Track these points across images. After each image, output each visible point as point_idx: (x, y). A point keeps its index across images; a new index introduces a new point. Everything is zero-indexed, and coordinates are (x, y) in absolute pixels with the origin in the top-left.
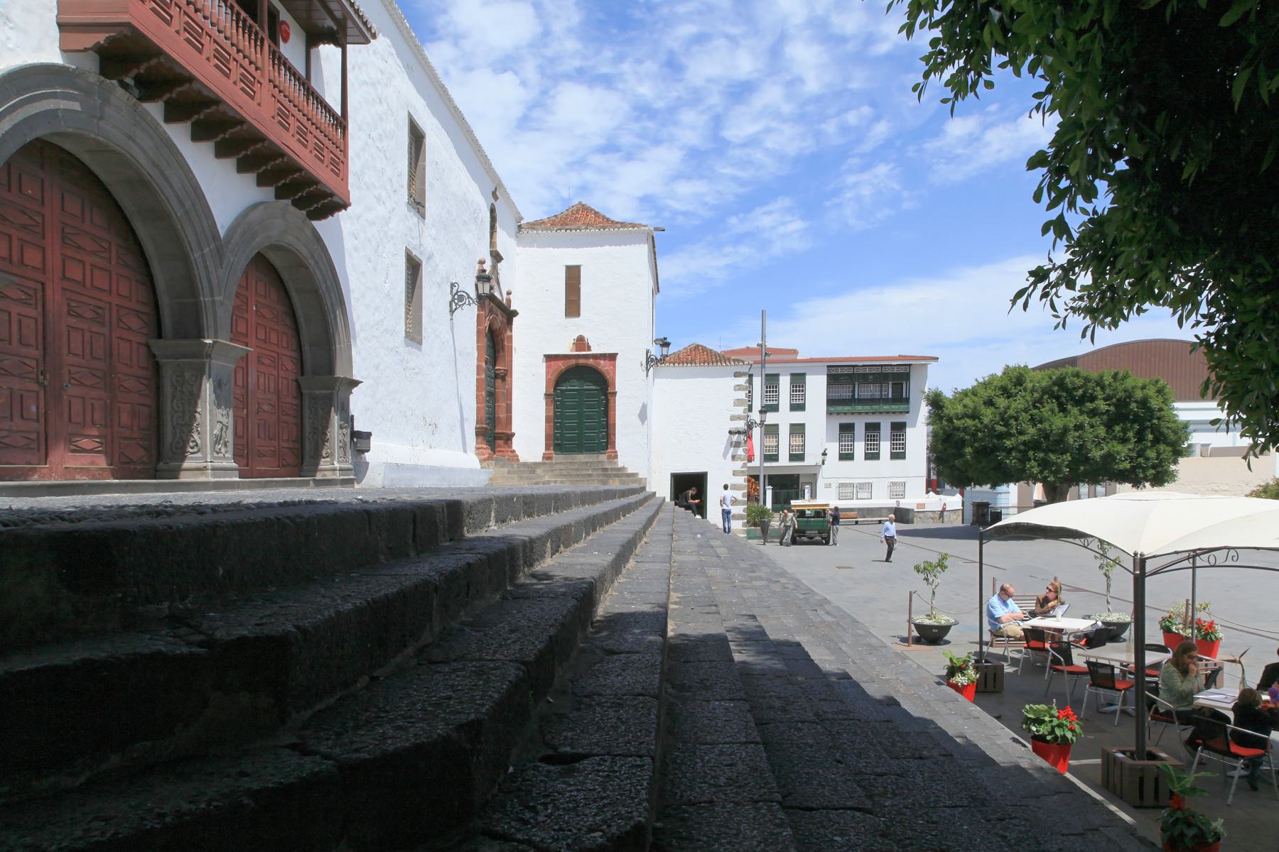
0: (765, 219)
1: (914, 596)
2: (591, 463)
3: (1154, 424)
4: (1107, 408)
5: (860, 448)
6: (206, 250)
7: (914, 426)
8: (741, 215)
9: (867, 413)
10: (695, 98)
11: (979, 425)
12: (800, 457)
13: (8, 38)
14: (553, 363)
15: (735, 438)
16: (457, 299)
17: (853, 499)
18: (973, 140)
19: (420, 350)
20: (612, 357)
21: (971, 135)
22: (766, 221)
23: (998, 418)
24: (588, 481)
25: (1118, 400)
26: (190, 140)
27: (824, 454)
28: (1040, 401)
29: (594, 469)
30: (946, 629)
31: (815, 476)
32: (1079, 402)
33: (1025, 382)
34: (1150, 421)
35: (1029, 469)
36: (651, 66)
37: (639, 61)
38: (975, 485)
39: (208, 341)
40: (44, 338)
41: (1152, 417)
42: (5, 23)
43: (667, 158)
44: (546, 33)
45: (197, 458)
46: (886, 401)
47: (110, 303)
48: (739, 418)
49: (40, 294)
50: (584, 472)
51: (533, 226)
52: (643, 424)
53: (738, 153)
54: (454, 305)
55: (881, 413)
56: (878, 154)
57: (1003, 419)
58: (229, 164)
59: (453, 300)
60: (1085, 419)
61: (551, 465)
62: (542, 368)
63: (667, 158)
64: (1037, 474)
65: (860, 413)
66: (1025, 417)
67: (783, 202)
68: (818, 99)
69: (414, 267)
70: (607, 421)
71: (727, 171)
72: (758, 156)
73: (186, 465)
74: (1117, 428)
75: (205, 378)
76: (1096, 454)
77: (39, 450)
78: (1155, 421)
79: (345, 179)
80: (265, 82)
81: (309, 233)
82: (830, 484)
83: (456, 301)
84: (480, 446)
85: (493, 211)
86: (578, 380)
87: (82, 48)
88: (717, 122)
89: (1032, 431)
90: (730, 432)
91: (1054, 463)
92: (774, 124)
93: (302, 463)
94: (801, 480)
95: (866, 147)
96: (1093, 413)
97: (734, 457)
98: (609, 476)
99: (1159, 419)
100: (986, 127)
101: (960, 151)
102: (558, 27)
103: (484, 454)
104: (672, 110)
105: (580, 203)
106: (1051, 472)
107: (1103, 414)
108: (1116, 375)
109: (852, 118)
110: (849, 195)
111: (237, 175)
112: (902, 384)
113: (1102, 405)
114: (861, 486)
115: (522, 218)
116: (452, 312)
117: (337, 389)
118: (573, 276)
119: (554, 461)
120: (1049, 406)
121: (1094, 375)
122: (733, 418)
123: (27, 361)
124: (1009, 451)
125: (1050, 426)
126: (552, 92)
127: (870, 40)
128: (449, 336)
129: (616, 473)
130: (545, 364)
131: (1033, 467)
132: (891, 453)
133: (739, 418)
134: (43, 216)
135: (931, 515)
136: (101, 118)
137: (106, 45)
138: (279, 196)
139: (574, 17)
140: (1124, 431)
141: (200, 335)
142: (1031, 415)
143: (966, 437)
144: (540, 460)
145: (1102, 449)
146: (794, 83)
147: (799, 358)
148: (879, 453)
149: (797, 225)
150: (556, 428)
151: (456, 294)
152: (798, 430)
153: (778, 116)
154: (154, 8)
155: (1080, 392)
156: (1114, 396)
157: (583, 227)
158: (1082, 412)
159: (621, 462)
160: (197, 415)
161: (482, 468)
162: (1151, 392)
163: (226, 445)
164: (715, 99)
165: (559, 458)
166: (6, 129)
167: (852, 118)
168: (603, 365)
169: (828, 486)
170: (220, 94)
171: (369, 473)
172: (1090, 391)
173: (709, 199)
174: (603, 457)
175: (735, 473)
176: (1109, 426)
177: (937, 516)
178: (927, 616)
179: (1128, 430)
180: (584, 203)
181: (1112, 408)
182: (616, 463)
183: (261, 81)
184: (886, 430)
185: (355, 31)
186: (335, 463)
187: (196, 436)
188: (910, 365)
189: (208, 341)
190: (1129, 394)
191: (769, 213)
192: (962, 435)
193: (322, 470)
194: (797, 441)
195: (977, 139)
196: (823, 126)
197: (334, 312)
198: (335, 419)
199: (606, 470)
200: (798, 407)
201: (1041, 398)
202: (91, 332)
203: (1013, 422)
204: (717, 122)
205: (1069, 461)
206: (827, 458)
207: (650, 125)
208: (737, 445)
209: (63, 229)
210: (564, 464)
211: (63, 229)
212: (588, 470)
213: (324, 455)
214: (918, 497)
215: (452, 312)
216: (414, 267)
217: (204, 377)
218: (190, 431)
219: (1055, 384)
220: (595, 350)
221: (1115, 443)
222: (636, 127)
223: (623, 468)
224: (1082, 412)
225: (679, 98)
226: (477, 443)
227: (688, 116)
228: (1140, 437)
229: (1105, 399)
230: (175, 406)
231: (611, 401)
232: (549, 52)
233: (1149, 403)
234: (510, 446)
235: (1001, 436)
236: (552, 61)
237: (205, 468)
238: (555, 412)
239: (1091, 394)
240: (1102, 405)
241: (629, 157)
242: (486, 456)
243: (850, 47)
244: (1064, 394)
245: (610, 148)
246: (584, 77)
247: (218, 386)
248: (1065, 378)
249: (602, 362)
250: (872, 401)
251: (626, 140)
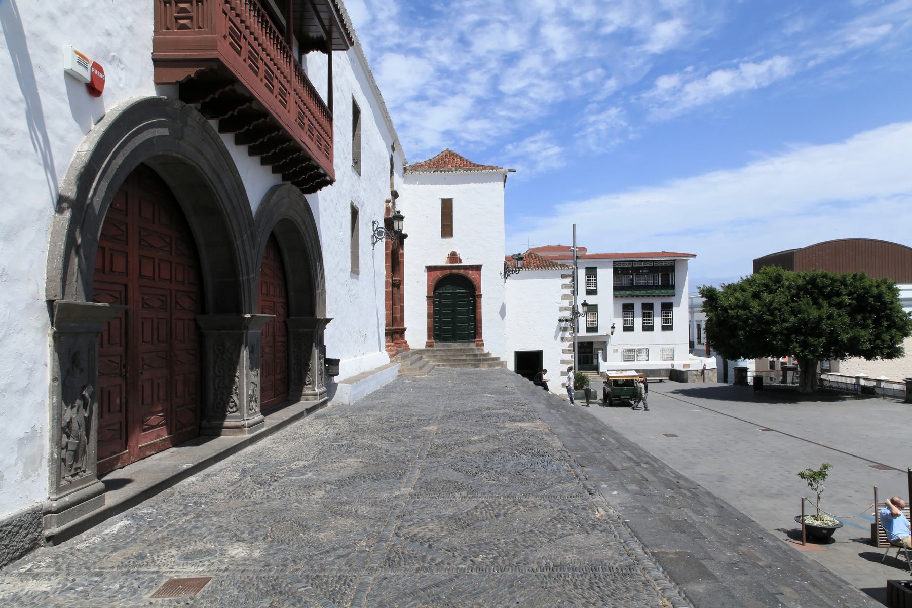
0: (532, 146)
1: (806, 502)
2: (465, 350)
3: (887, 313)
4: (850, 301)
5: (638, 322)
6: (245, 237)
7: (679, 305)
8: (515, 144)
9: (643, 296)
10: (479, 64)
11: (749, 314)
12: (595, 330)
13: (120, 79)
14: (432, 272)
15: (563, 324)
16: (377, 234)
17: (634, 361)
18: (676, 91)
19: (358, 279)
20: (478, 268)
21: (674, 87)
22: (533, 148)
23: (765, 309)
24: (464, 364)
25: (858, 295)
26: (234, 144)
27: (613, 327)
28: (797, 295)
29: (467, 355)
30: (832, 530)
31: (605, 343)
32: (828, 297)
33: (782, 280)
34: (884, 311)
35: (792, 349)
36: (448, 42)
37: (440, 39)
38: (745, 358)
39: (248, 316)
40: (126, 333)
41: (885, 309)
42: (118, 65)
43: (460, 104)
44: (374, 20)
45: (236, 417)
46: (657, 287)
47: (171, 290)
48: (566, 309)
49: (123, 294)
50: (459, 358)
51: (416, 167)
52: (503, 319)
53: (511, 101)
54: (375, 238)
55: (654, 296)
56: (611, 101)
57: (769, 310)
58: (257, 159)
59: (374, 234)
60: (835, 311)
61: (433, 351)
62: (424, 276)
63: (460, 104)
64: (799, 353)
65: (638, 296)
66: (786, 309)
67: (544, 135)
68: (565, 64)
69: (355, 213)
70: (475, 317)
71: (504, 113)
72: (525, 103)
73: (227, 423)
74: (859, 317)
75: (243, 346)
76: (844, 337)
77: (120, 439)
78: (888, 311)
79: (331, 161)
80: (292, 92)
81: (302, 204)
82: (617, 350)
83: (377, 235)
84: (389, 344)
85: (392, 160)
86: (452, 285)
87: (174, 81)
88: (496, 80)
89: (793, 319)
90: (560, 320)
91: (813, 345)
92: (535, 81)
93: (288, 390)
94: (595, 346)
95: (601, 97)
96: (840, 305)
97: (562, 339)
98: (480, 360)
99: (890, 309)
100: (685, 82)
101: (667, 99)
102: (382, 16)
103: (392, 351)
104: (464, 72)
105: (447, 150)
106: (810, 351)
107: (848, 306)
108: (855, 276)
109: (590, 76)
110: (591, 129)
111: (261, 166)
112: (669, 274)
113: (847, 300)
114: (641, 351)
115: (407, 163)
116: (374, 244)
117: (317, 327)
118: (447, 206)
119: (435, 348)
120: (805, 302)
121: (838, 276)
122: (561, 309)
123: (113, 359)
124: (775, 335)
125: (808, 316)
126: (379, 60)
127: (599, 24)
128: (371, 263)
129: (484, 358)
130: (426, 273)
131: (796, 348)
132: (662, 326)
133: (566, 309)
134: (127, 225)
135: (695, 373)
136: (181, 139)
137: (195, 78)
138: (284, 179)
139: (394, 9)
140: (864, 319)
141: (239, 311)
142: (791, 307)
143: (739, 323)
144: (423, 347)
145: (848, 333)
146: (548, 53)
147: (588, 254)
148: (653, 326)
149: (555, 150)
150: (435, 322)
151: (377, 229)
152: (592, 309)
153: (537, 75)
154: (231, 42)
155: (829, 289)
156: (855, 292)
157: (454, 169)
158: (830, 305)
159: (486, 349)
160: (236, 379)
161: (391, 362)
162: (883, 288)
163: (256, 401)
164: (493, 65)
165: (438, 346)
166: (120, 163)
167: (590, 76)
168: (471, 274)
169: (616, 351)
170: (269, 109)
171: (338, 393)
172: (836, 289)
173: (491, 133)
174: (472, 345)
175: (564, 351)
176: (851, 314)
177: (700, 374)
178: (813, 516)
179: (867, 318)
180: (450, 150)
181: (854, 302)
182: (482, 349)
183: (290, 92)
184: (657, 308)
185: (341, 41)
186: (316, 389)
187: (235, 398)
188: (674, 261)
189: (248, 316)
190: (867, 290)
191: (535, 142)
192: (736, 321)
193: (305, 395)
194: (592, 317)
195: (679, 90)
196: (570, 82)
197: (316, 265)
198: (316, 352)
199: (476, 355)
200: (592, 292)
201: (798, 294)
202: (157, 318)
203: (777, 312)
204: (496, 80)
205: (824, 343)
206: (615, 330)
207: (449, 82)
208: (565, 329)
209: (140, 232)
210: (443, 350)
211: (140, 232)
212: (462, 355)
213: (307, 382)
214: (685, 360)
215: (374, 244)
216: (355, 213)
217: (243, 346)
218: (230, 393)
219: (808, 283)
220: (465, 263)
221: (859, 329)
222: (439, 83)
223: (488, 354)
224: (830, 305)
225: (468, 64)
226: (386, 342)
227: (475, 76)
228: (877, 323)
229: (848, 295)
230: (217, 373)
231: (478, 301)
232: (376, 33)
233: (884, 297)
234: (403, 339)
235: (768, 323)
236: (378, 39)
237: (243, 426)
238: (434, 310)
239: (837, 291)
240: (847, 300)
241: (434, 104)
242: (394, 352)
243: (586, 29)
244: (816, 291)
245: (420, 97)
246: (399, 49)
247: (252, 352)
248: (816, 279)
249: (470, 272)
250: (646, 287)
251: (432, 92)
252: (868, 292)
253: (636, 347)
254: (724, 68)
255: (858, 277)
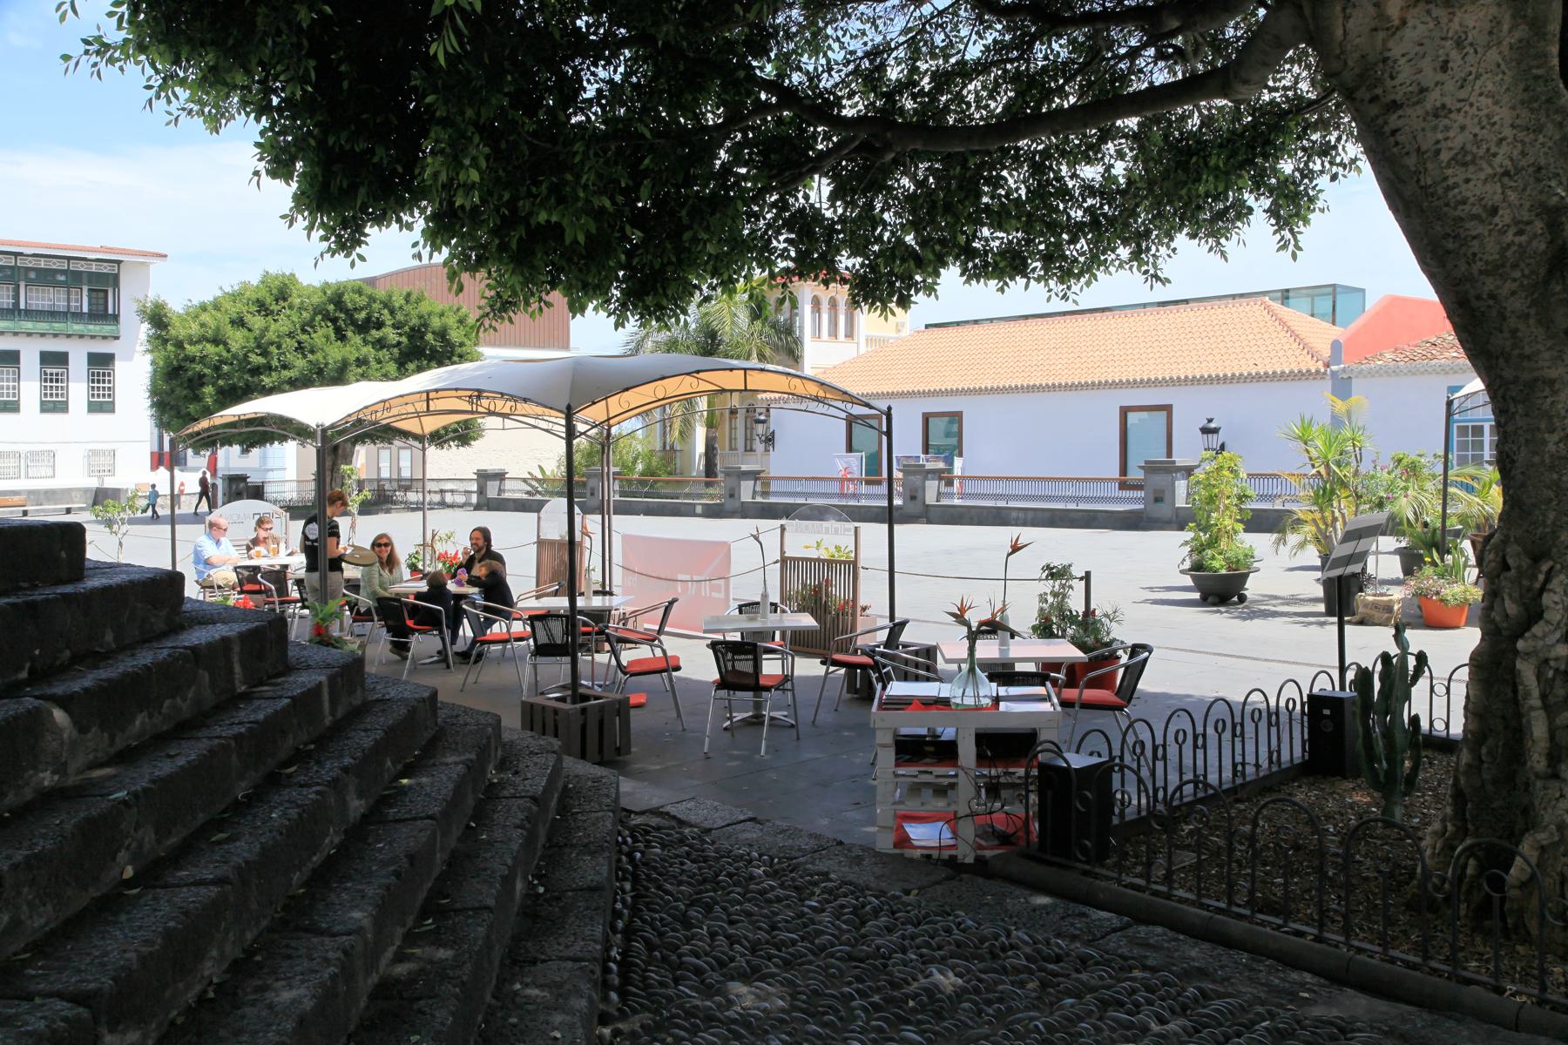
9: (43, 335)
11: (225, 354)
28: (311, 323)
46: (78, 316)
55: (69, 336)
65: (29, 334)
66: (290, 344)
96: (380, 344)
107: (394, 346)
108: (409, 295)
112: (106, 292)
113: (391, 335)
114: (34, 456)
155: (363, 315)
158: (366, 342)
184: (78, 363)
201: (313, 319)
219: (331, 301)
224: (366, 342)
229: (394, 326)
240: (391, 335)
250: (52, 315)
252: (425, 325)
253: (23, 448)
254: (1484, 596)
255: (413, 298)
